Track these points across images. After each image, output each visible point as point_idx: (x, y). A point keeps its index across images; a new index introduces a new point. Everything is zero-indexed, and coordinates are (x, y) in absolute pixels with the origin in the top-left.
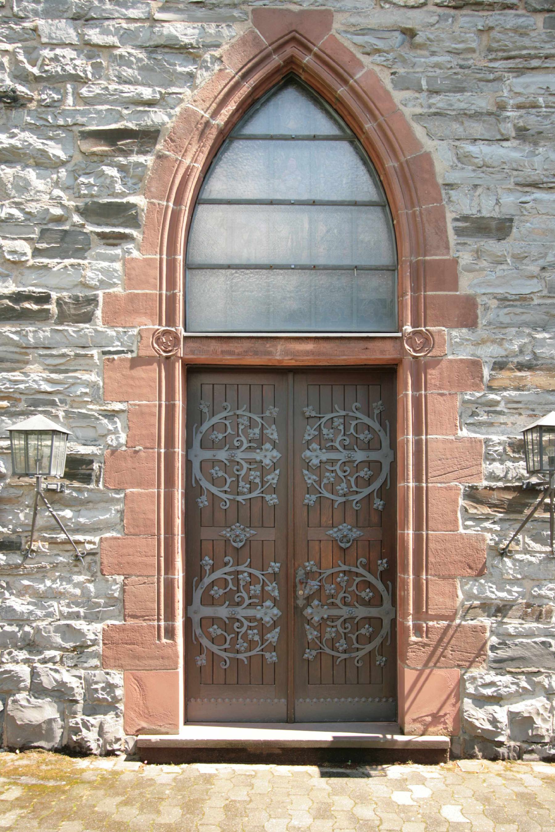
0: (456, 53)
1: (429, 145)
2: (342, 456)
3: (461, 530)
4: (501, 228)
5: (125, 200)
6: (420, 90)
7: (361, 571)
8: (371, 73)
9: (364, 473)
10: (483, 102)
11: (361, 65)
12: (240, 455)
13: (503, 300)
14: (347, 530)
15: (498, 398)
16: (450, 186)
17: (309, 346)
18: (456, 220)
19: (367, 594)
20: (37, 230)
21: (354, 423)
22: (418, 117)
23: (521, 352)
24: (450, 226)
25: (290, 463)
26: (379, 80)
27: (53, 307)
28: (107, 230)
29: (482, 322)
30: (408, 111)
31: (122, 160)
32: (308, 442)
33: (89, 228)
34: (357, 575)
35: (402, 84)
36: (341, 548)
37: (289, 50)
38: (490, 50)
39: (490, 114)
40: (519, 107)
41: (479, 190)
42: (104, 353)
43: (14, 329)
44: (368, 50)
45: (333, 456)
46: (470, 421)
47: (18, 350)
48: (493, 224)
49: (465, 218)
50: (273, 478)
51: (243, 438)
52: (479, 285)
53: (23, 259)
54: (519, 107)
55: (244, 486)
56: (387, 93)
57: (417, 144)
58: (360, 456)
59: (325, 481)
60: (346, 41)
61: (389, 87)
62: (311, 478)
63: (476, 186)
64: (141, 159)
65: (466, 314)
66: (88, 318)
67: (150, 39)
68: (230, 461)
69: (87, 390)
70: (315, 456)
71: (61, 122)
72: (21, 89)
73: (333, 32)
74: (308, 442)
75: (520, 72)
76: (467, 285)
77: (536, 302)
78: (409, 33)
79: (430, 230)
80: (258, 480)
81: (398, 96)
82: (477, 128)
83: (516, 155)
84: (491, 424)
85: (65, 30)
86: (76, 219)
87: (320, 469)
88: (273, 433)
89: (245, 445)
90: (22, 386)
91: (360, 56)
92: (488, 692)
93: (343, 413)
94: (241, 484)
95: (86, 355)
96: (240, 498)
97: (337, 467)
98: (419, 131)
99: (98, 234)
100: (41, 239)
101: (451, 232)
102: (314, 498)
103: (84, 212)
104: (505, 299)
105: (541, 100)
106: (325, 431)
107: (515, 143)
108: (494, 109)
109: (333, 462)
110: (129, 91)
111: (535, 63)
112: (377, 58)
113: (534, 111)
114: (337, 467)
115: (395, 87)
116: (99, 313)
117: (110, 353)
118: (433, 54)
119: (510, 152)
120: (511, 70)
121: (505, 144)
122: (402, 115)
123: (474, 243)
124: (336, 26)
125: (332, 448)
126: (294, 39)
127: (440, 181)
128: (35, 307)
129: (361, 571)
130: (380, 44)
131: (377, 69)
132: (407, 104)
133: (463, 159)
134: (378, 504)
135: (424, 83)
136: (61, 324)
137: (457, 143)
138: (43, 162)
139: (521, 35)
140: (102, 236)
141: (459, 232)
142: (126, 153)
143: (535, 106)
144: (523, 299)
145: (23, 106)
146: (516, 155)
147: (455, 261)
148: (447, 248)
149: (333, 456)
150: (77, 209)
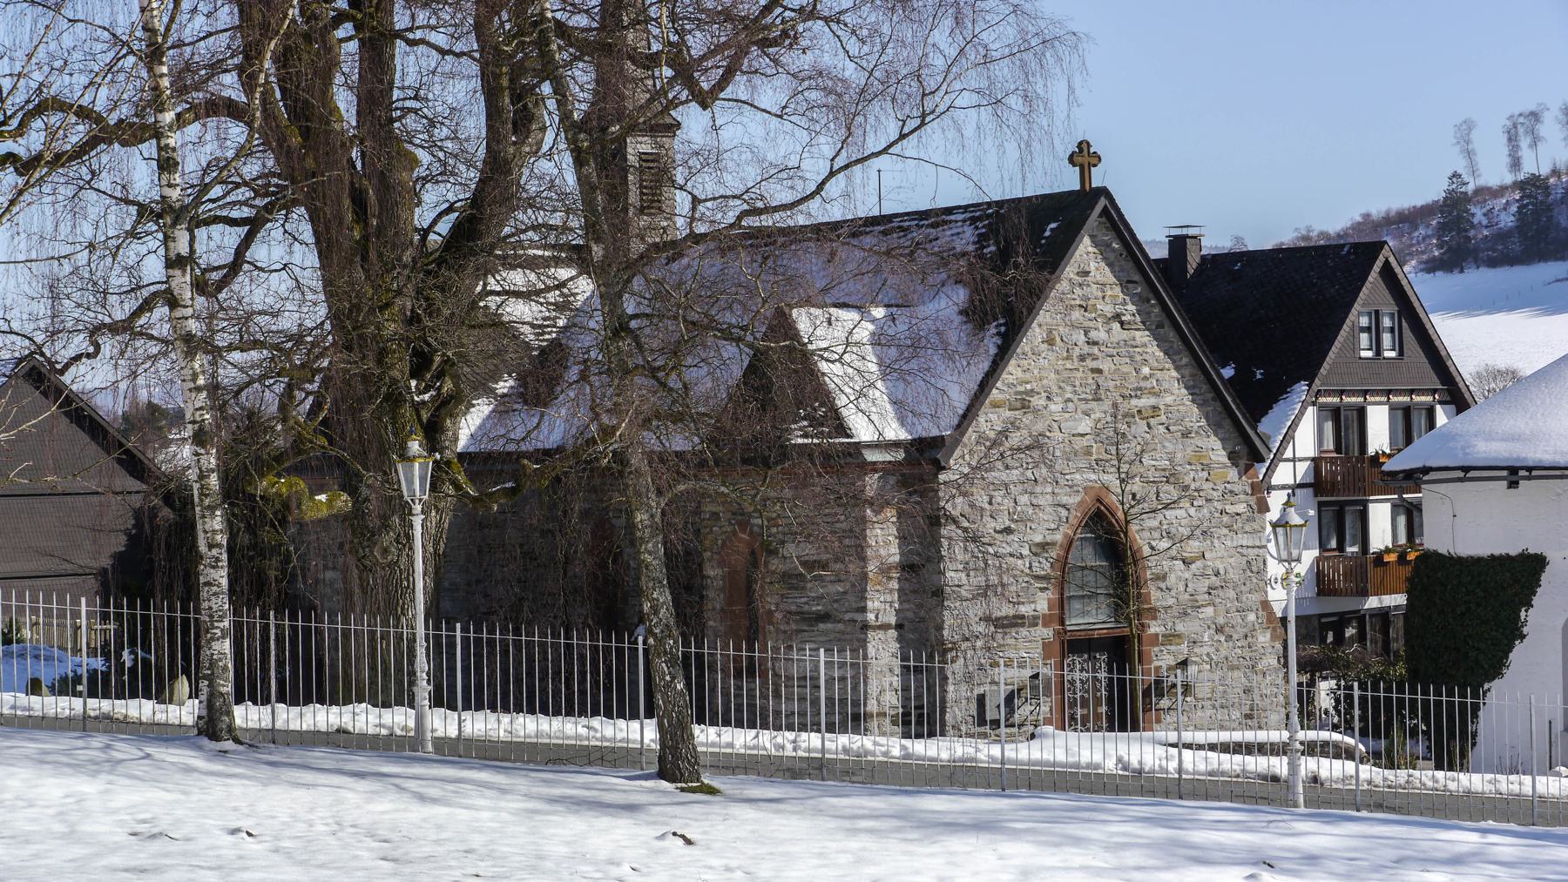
66: (1036, 625)
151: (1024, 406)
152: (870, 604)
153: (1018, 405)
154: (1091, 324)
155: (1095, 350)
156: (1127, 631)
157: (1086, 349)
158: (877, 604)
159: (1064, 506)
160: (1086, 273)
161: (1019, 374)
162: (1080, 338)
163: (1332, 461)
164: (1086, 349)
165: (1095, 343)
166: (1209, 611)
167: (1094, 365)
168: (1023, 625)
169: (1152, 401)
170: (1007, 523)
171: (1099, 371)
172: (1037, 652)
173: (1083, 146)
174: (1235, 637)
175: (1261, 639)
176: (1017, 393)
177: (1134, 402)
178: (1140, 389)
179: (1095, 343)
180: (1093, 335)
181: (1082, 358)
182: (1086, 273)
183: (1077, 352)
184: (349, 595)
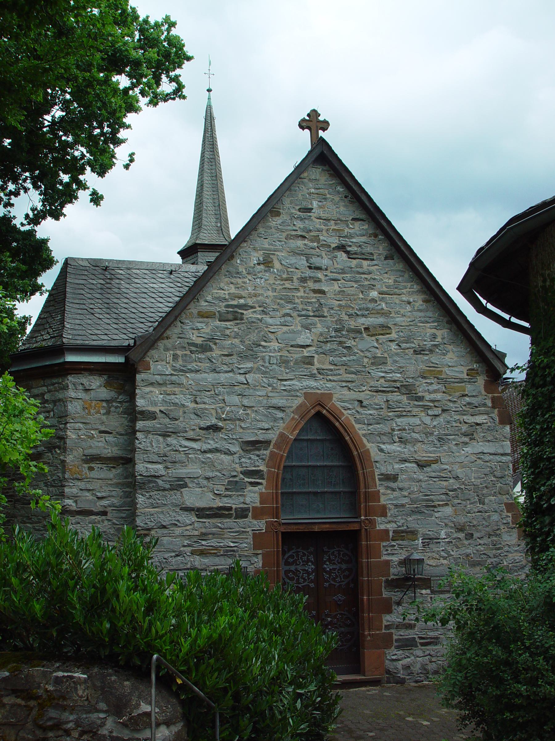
0: (377, 409)
1: (369, 445)
2: (337, 567)
3: (384, 596)
4: (393, 478)
5: (259, 469)
6: (365, 424)
7: (345, 613)
8: (347, 417)
9: (347, 573)
10: (387, 429)
11: (343, 414)
12: (299, 568)
13: (396, 506)
14: (340, 597)
15: (395, 544)
16: (377, 462)
17: (327, 526)
18: (379, 475)
19: (349, 622)
20: (227, 481)
21: (342, 553)
22: (364, 435)
23: (403, 526)
24: (377, 477)
25: (319, 570)
26: (350, 420)
27: (233, 512)
28: (253, 480)
29: (389, 514)
30: (361, 432)
31: (257, 453)
32: (325, 561)
33: (246, 480)
34: (345, 615)
35: (358, 421)
36: (338, 604)
37: (318, 408)
38: (389, 408)
39: (389, 433)
40: (399, 430)
41: (386, 463)
42: (253, 530)
43: (219, 521)
44: (346, 408)
45: (334, 567)
46: (386, 553)
47: (220, 530)
48: (392, 476)
49: (382, 474)
50: (312, 577)
51: (301, 561)
52: (388, 500)
53: (222, 493)
54: (399, 430)
55: (301, 580)
56: (353, 425)
57: (364, 446)
58: (344, 566)
59: (332, 577)
60: (338, 404)
61: (354, 423)
62: (326, 576)
63: (385, 462)
64: (265, 452)
65: (384, 514)
66: (246, 516)
67: (267, 404)
68: (295, 570)
69: (246, 546)
70: (328, 567)
71: (234, 437)
72: (220, 424)
73: (333, 401)
74: (325, 561)
75: (399, 416)
76: (383, 500)
77: (407, 506)
78: (361, 402)
79: (370, 480)
80: (306, 578)
81: (357, 426)
82: (385, 438)
83: (398, 449)
84: (393, 554)
85: (236, 399)
86: (242, 476)
87: (329, 573)
88: (312, 558)
89: (301, 563)
90: (222, 544)
91: (343, 411)
92: (394, 657)
93: (338, 549)
94: (300, 579)
95: (245, 532)
96: (300, 586)
97: (336, 572)
98: (365, 440)
99: (249, 482)
100: (228, 484)
101: (377, 480)
102: (327, 584)
103: (243, 473)
104: (397, 506)
105: (407, 427)
106: (331, 557)
107: (398, 444)
108: (390, 431)
109: (334, 569)
110: (260, 425)
111: (404, 413)
112: (350, 412)
113: (404, 431)
114: (336, 572)
115: (356, 423)
116: (250, 514)
117: (255, 530)
118: (369, 410)
119: (396, 447)
120: (396, 416)
121: (395, 444)
122: (358, 434)
123: (385, 483)
124: (334, 399)
125: (334, 564)
126: (319, 404)
127: (373, 460)
128: (227, 513)
129: (345, 613)
130: (350, 407)
131: (349, 416)
132: (360, 430)
133: (381, 450)
134: (352, 585)
135: (366, 421)
136: (236, 519)
137: (378, 444)
138: (229, 453)
139: (399, 403)
140: (251, 483)
141: (380, 480)
142: (259, 450)
143: (404, 430)
144: (403, 506)
145: (220, 431)
146: (398, 449)
147: (379, 491)
148: (376, 486)
149: (334, 567)
150: (241, 473)
151: (236, 317)
152: (67, 490)
153: (230, 317)
154: (313, 252)
155: (320, 275)
156: (251, 533)
157: (309, 273)
158: (75, 491)
159: (279, 408)
160: (310, 210)
161: (233, 290)
162: (303, 262)
163: (17, 351)
164: (309, 273)
165: (319, 268)
166: (448, 510)
167: (317, 286)
168: (229, 516)
169: (381, 320)
170: (214, 421)
171: (323, 292)
172: (246, 544)
173: (314, 114)
174: (476, 535)
175: (506, 537)
176: (227, 306)
177: (362, 320)
178: (367, 309)
179: (319, 268)
180: (315, 261)
181: (303, 280)
182: (310, 210)
183: (298, 274)
184: (323, 455)
